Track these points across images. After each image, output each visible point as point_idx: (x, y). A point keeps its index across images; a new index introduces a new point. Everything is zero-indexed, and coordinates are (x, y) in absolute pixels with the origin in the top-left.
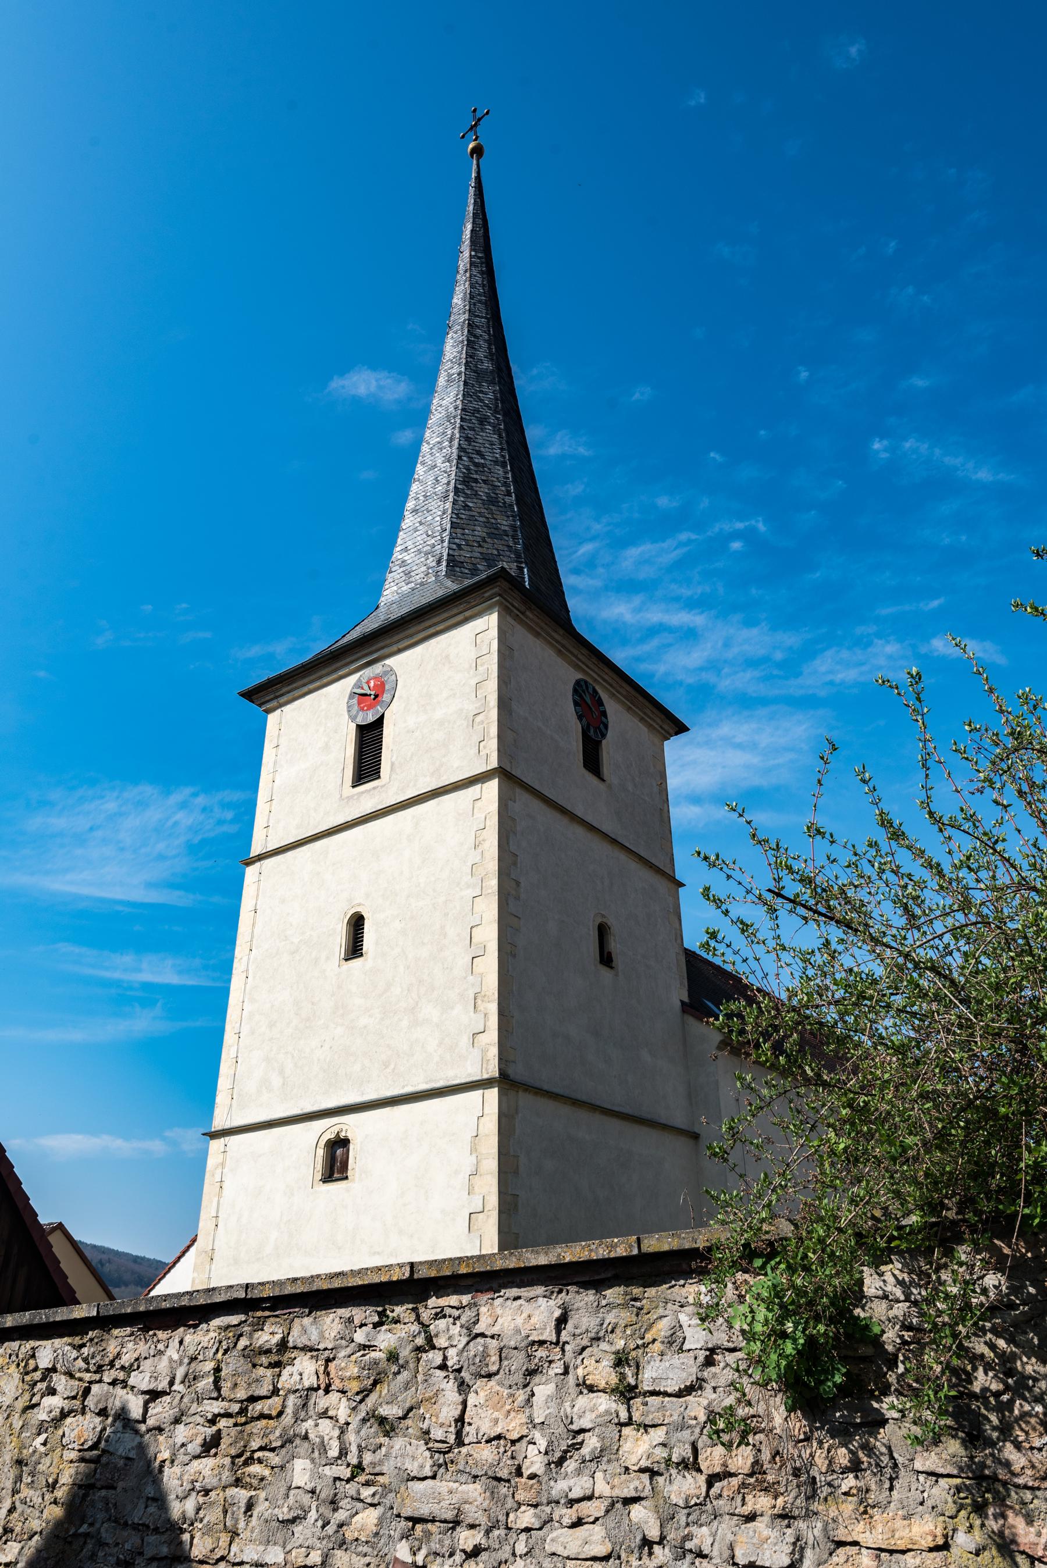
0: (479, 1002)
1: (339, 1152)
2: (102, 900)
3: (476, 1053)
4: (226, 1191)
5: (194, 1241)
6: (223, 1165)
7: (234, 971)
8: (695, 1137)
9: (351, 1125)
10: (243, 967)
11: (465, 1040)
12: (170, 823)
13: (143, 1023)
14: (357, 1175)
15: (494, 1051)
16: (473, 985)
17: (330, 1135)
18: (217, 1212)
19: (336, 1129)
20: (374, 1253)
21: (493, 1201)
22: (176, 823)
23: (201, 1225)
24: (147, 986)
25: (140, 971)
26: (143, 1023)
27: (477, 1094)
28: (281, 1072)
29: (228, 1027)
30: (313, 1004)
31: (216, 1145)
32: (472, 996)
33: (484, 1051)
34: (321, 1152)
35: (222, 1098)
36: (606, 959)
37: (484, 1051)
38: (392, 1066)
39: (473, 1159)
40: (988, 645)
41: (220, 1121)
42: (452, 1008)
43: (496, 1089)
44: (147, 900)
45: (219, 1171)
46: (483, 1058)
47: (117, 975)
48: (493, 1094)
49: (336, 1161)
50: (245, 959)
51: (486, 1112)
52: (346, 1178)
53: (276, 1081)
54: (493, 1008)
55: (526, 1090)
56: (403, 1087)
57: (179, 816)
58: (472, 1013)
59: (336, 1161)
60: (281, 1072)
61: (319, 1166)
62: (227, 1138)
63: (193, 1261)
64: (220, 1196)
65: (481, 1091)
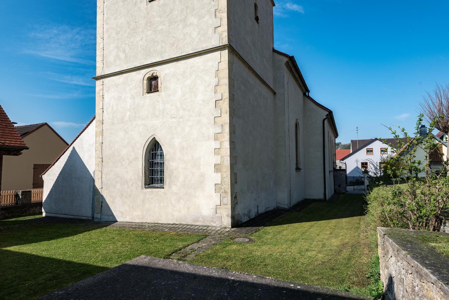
0: (217, 13)
1: (153, 82)
2: (58, 60)
3: (217, 36)
4: (106, 99)
5: (94, 118)
6: (103, 89)
7: (97, 13)
8: (275, 93)
9: (158, 71)
10: (101, 10)
11: (211, 31)
12: (74, 38)
13: (76, 95)
14: (163, 89)
15: (226, 34)
16: (214, 6)
17: (149, 75)
18: (103, 106)
19: (151, 73)
20: (173, 118)
21: (226, 95)
22: (76, 39)
23: (96, 112)
24: (76, 85)
25: (73, 81)
26: (76, 95)
27: (217, 54)
28: (124, 52)
29: (98, 36)
30: (136, 22)
31: (98, 83)
32: (214, 11)
33: (221, 35)
34: (145, 82)
35: (99, 64)
36: (257, 19)
37: (221, 35)
38: (176, 45)
39: (217, 79)
40: (300, 7)
41: (99, 73)
42: (204, 17)
43: (227, 50)
44: (71, 61)
45: (101, 92)
46: (221, 37)
47: (66, 81)
48: (225, 53)
49: (152, 85)
50: (102, 6)
51: (222, 60)
52: (158, 91)
53: (122, 56)
54: (225, 15)
55: (236, 55)
56: (182, 53)
57: (77, 36)
58: (214, 19)
59: (152, 85)
60: (124, 52)
61: (145, 87)
62: (103, 80)
63: (95, 125)
64: (103, 101)
65: (220, 52)
